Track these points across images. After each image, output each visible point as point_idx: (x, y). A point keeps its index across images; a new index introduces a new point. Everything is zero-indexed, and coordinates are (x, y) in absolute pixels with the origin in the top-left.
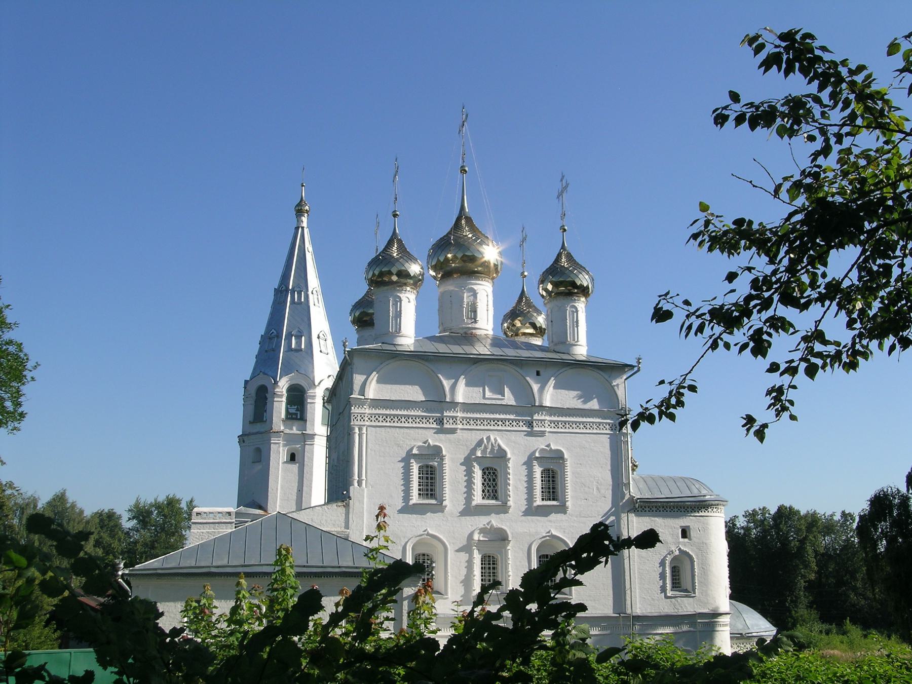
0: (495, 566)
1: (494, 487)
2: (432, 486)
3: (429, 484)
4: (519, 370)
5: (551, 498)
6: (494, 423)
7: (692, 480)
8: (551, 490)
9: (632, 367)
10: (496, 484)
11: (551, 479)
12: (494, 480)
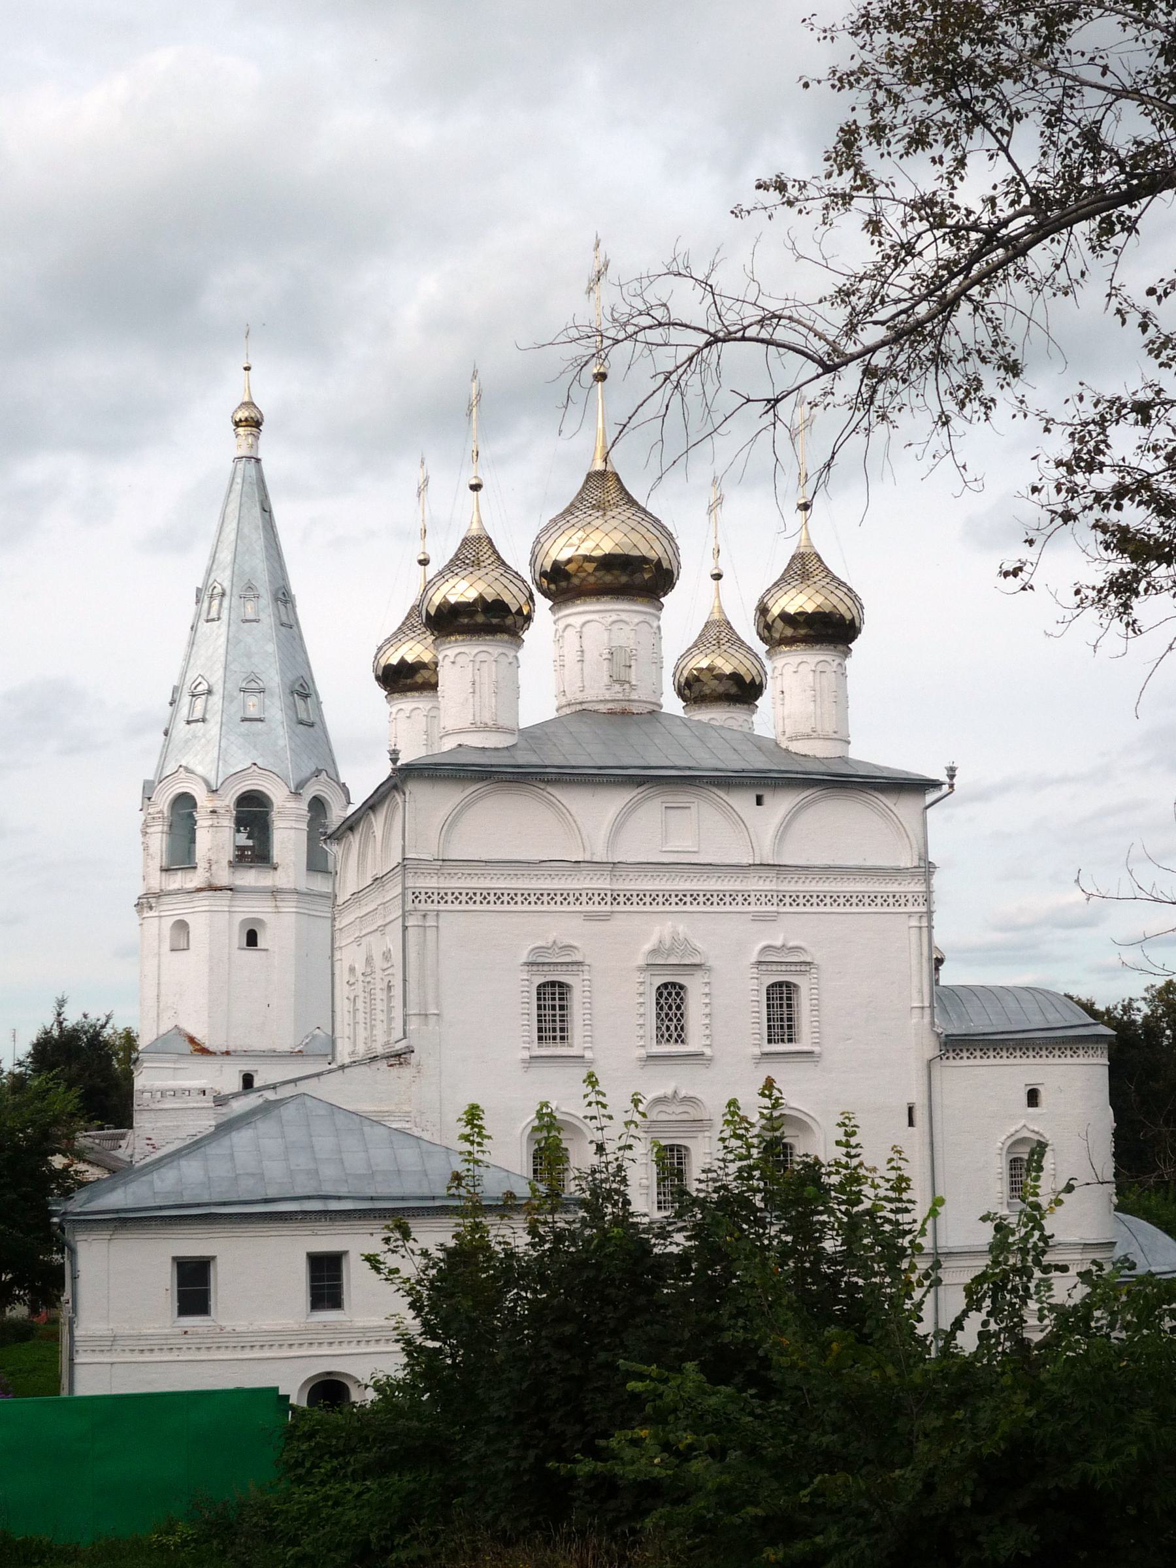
0: (565, 1003)
1: (679, 1020)
2: (563, 1021)
3: (558, 1018)
4: (725, 797)
5: (786, 1037)
6: (677, 900)
7: (1049, 996)
8: (786, 1023)
9: (935, 785)
10: (682, 1015)
11: (785, 1002)
12: (678, 1008)
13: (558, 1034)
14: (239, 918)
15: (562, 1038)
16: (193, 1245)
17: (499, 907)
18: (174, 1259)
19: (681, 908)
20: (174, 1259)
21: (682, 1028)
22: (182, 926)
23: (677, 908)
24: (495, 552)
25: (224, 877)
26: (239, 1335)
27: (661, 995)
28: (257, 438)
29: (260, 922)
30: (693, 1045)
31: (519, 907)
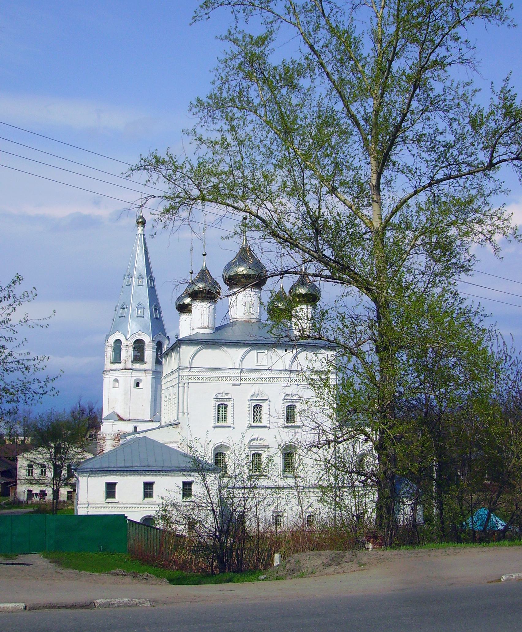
12: (260, 412)
13: (224, 419)
14: (133, 379)
15: (225, 420)
16: (111, 479)
17: (207, 381)
18: (106, 482)
19: (261, 382)
20: (106, 482)
21: (261, 418)
22: (116, 380)
23: (260, 382)
24: (211, 276)
25: (129, 365)
26: (124, 504)
27: (255, 408)
28: (144, 228)
29: (141, 380)
30: (265, 422)
31: (213, 381)
